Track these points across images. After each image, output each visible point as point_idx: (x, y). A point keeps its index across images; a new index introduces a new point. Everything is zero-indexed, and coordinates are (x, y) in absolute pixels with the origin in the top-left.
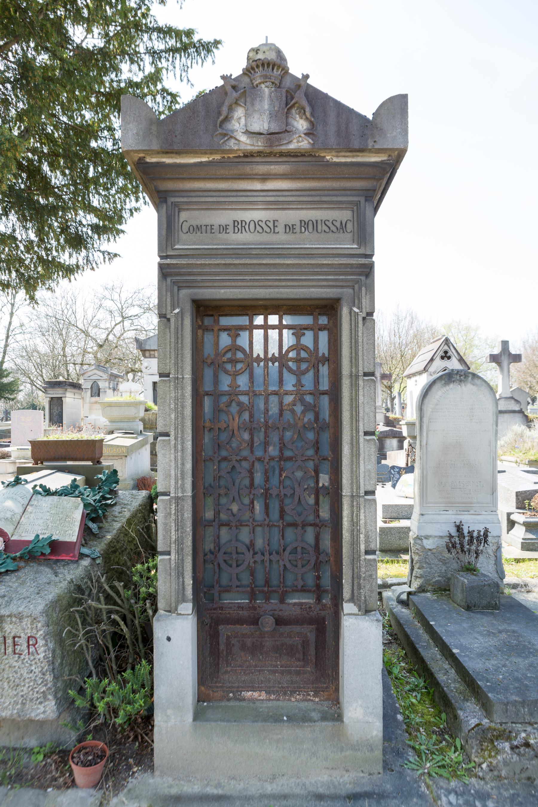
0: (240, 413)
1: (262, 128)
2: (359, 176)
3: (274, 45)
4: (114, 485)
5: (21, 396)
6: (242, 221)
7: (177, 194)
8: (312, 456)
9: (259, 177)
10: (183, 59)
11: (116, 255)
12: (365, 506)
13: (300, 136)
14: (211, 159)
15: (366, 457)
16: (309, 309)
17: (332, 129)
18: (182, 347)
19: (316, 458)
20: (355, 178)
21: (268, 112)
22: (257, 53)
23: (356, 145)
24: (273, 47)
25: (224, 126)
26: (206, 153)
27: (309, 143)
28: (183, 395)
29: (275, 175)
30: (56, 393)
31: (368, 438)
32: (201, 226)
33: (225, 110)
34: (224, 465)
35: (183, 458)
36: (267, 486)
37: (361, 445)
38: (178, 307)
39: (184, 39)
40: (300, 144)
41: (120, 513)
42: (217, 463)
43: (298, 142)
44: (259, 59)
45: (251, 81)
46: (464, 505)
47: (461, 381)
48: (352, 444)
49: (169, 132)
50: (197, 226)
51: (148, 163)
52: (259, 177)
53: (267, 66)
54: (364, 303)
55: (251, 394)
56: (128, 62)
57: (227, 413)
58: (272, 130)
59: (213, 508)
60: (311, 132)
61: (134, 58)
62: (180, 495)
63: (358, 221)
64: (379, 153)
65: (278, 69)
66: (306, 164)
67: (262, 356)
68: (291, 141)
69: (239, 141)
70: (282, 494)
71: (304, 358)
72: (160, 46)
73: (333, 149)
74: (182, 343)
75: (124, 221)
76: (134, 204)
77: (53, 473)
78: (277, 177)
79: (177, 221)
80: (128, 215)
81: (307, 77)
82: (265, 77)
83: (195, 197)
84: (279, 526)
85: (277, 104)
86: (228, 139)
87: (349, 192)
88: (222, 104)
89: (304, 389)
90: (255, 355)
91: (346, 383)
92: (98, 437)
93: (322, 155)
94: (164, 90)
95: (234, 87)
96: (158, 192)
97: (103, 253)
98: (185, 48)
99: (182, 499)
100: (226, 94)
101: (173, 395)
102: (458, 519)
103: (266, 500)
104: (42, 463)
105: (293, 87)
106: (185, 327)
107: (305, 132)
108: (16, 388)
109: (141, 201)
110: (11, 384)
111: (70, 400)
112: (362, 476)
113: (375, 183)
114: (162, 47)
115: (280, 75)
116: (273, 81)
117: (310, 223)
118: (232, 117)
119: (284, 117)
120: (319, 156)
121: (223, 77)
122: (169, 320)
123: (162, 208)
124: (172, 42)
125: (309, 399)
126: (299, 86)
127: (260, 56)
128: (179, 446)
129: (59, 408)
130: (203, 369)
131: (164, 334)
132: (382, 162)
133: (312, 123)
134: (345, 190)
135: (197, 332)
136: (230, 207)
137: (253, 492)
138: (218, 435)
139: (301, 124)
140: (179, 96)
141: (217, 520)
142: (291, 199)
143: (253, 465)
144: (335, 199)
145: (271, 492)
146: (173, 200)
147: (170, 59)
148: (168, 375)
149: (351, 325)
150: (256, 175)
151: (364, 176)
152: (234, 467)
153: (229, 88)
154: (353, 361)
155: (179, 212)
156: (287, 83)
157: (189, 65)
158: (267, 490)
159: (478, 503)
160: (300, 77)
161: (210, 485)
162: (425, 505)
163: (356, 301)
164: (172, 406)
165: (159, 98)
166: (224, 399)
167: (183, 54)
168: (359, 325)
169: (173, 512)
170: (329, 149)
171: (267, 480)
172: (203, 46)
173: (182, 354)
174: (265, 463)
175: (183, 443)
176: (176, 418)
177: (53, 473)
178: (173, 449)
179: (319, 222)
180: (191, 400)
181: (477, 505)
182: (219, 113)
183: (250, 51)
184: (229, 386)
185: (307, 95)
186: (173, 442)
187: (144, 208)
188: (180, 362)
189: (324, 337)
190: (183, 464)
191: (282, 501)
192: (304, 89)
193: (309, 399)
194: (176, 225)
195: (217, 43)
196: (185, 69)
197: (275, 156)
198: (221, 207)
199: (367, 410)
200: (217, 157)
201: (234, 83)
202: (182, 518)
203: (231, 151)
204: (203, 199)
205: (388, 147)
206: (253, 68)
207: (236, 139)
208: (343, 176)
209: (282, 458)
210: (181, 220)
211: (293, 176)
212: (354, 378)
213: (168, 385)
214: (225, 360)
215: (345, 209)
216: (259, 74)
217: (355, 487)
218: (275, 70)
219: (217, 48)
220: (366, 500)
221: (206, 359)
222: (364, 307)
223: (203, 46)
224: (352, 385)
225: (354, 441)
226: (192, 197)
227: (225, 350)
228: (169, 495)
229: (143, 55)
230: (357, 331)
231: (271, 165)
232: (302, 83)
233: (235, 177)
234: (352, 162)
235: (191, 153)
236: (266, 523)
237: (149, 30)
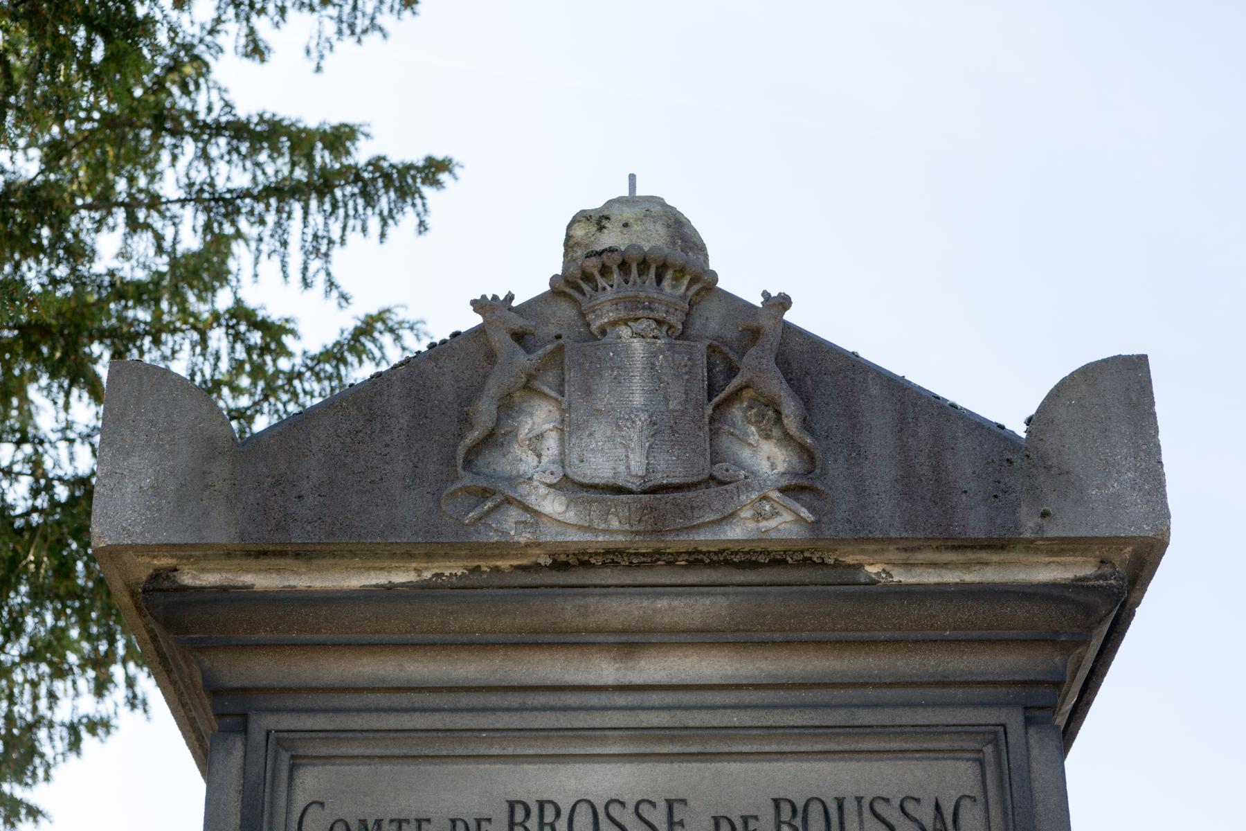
1: (622, 468)
2: (993, 634)
3: (659, 201)
6: (541, 804)
7: (290, 702)
9: (612, 639)
10: (317, 219)
13: (765, 498)
14: (427, 575)
17: (882, 471)
20: (982, 641)
21: (644, 416)
22: (601, 228)
23: (976, 524)
24: (656, 209)
25: (481, 462)
26: (409, 556)
27: (800, 520)
29: (671, 631)
32: (378, 822)
33: (485, 413)
39: (322, 156)
40: (764, 524)
43: (759, 516)
44: (611, 250)
45: (582, 315)
49: (277, 483)
50: (363, 822)
51: (185, 589)
52: (612, 639)
53: (635, 269)
56: (122, 229)
58: (659, 478)
60: (806, 483)
61: (141, 210)
63: (1003, 802)
64: (1062, 552)
65: (676, 279)
66: (793, 590)
68: (733, 515)
69: (536, 513)
72: (233, 176)
73: (891, 540)
75: (40, 772)
76: (88, 705)
78: (682, 637)
79: (282, 802)
80: (61, 746)
81: (784, 302)
82: (634, 303)
83: (359, 711)
85: (677, 392)
86: (497, 507)
87: (959, 693)
88: (479, 389)
93: (850, 560)
94: (241, 314)
95: (519, 337)
96: (216, 692)
98: (323, 185)
100: (491, 356)
105: (732, 334)
107: (784, 482)
109: (118, 693)
113: (1057, 659)
114: (241, 180)
115: (684, 297)
116: (661, 315)
117: (815, 809)
118: (513, 433)
119: (704, 434)
120: (837, 564)
121: (480, 305)
123: (229, 753)
124: (275, 167)
126: (754, 334)
127: (611, 238)
132: (1078, 585)
133: (803, 449)
134: (943, 683)
136: (496, 751)
139: (768, 458)
140: (293, 332)
142: (735, 719)
144: (906, 717)
146: (271, 722)
147: (271, 218)
150: (599, 631)
151: (1012, 634)
153: (501, 340)
155: (292, 768)
156: (711, 321)
157: (335, 233)
160: (757, 301)
165: (218, 338)
167: (314, 204)
170: (876, 540)
172: (387, 177)
179: (850, 808)
182: (465, 421)
183: (575, 221)
185: (783, 362)
187: (127, 720)
192: (771, 341)
194: (280, 818)
195: (434, 169)
196: (318, 247)
197: (670, 564)
198: (460, 751)
200: (453, 569)
201: (519, 323)
203: (505, 548)
204: (392, 721)
205: (1097, 532)
206: (587, 277)
207: (526, 508)
208: (932, 634)
210: (300, 801)
211: (743, 637)
215: (952, 753)
216: (610, 293)
218: (666, 283)
219: (436, 183)
223: (387, 177)
226: (348, 711)
229: (175, 208)
231: (659, 596)
232: (766, 323)
233: (518, 638)
234: (964, 584)
235: (354, 554)
237: (206, 131)
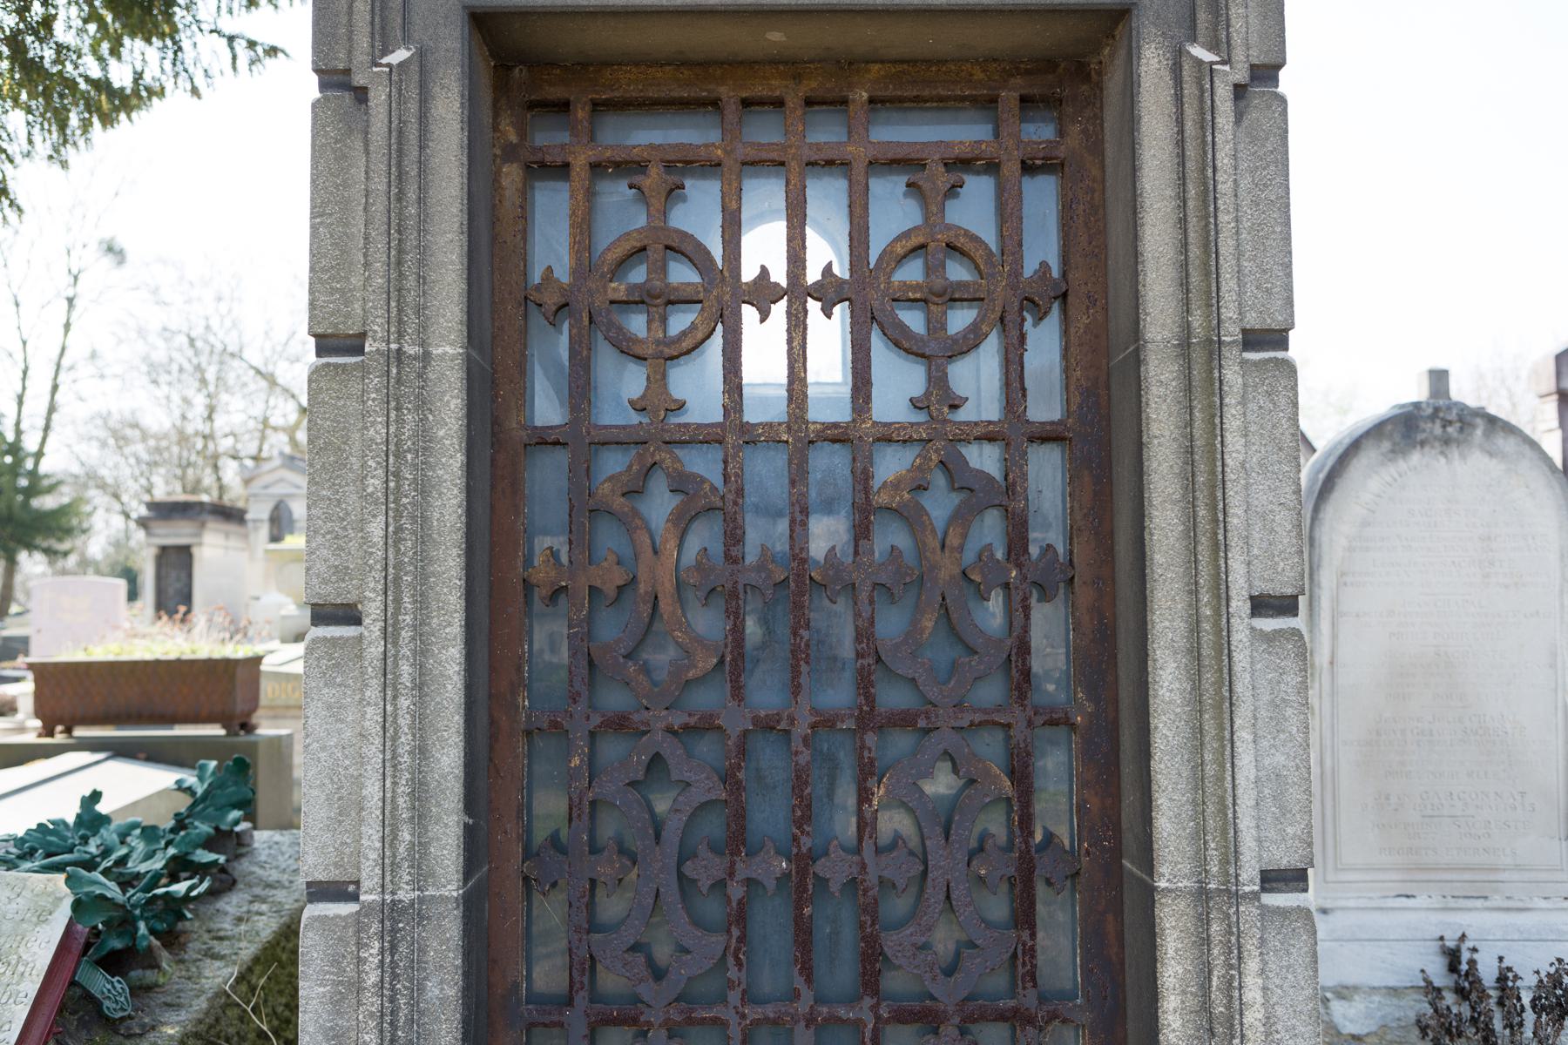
0: (683, 522)
4: (235, 814)
5: (96, 547)
8: (999, 709)
11: (273, 51)
12: (1263, 941)
15: (1263, 713)
16: (979, 75)
18: (423, 219)
19: (1017, 717)
28: (424, 436)
30: (175, 534)
31: (1268, 624)
34: (612, 749)
35: (422, 723)
36: (807, 843)
37: (1241, 659)
38: (406, 41)
41: (240, 920)
42: (582, 743)
46: (1467, 876)
47: (1447, 441)
48: (1195, 653)
54: (1237, 24)
55: (730, 439)
57: (631, 523)
59: (564, 944)
62: (405, 895)
67: (779, 276)
70: (872, 878)
71: (961, 285)
74: (421, 201)
77: (97, 763)
84: (858, 1024)
89: (963, 415)
90: (748, 273)
91: (1161, 379)
92: (239, 651)
97: (231, 39)
99: (417, 912)
101: (377, 432)
102: (1452, 924)
103: (799, 907)
104: (68, 731)
106: (436, 130)
108: (75, 522)
110: (62, 511)
111: (214, 551)
112: (1246, 799)
122: (361, 94)
125: (985, 459)
128: (406, 669)
129: (183, 575)
130: (524, 331)
131: (341, 157)
135: (498, 173)
137: (742, 871)
138: (590, 619)
141: (581, 999)
143: (742, 751)
145: (820, 867)
148: (354, 345)
149: (1180, 122)
152: (656, 760)
154: (1195, 278)
158: (803, 862)
159: (1518, 868)
161: (554, 841)
162: (1330, 877)
163: (1203, 17)
164: (375, 484)
166: (613, 463)
168: (1220, 121)
169: (373, 978)
171: (804, 814)
173: (423, 251)
174: (797, 744)
175: (422, 652)
176: (393, 538)
177: (97, 763)
178: (375, 684)
180: (460, 458)
181: (1516, 876)
184: (639, 406)
186: (375, 651)
188: (411, 282)
189: (1041, 199)
190: (422, 751)
191: (871, 910)
193: (985, 459)
199: (1261, 499)
202: (413, 1004)
209: (869, 718)
212: (1198, 356)
213: (356, 388)
214: (622, 296)
217: (1213, 853)
220: (1267, 912)
221: (538, 288)
222: (1237, 39)
224: (1188, 389)
225: (1207, 639)
227: (619, 252)
228: (354, 897)
230: (1208, 148)
236: (803, 1007)
